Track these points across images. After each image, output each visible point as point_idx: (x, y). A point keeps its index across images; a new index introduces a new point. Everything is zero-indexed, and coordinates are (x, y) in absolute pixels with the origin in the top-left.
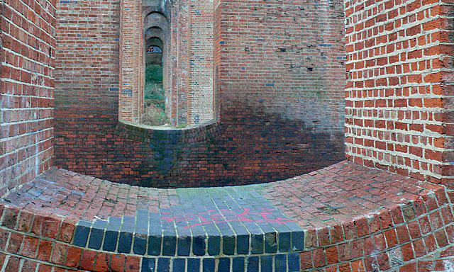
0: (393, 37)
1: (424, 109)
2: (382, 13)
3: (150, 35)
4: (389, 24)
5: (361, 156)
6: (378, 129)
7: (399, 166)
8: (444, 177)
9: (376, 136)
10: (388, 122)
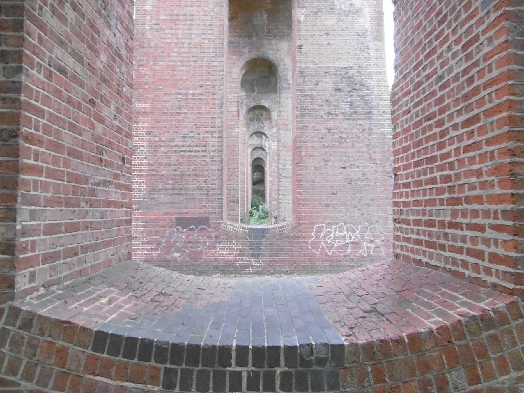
0: (443, 134)
1: (486, 206)
2: (431, 111)
3: (256, 164)
4: (439, 121)
5: (409, 254)
6: (427, 228)
7: (453, 268)
8: (518, 287)
9: (425, 235)
10: (439, 221)
